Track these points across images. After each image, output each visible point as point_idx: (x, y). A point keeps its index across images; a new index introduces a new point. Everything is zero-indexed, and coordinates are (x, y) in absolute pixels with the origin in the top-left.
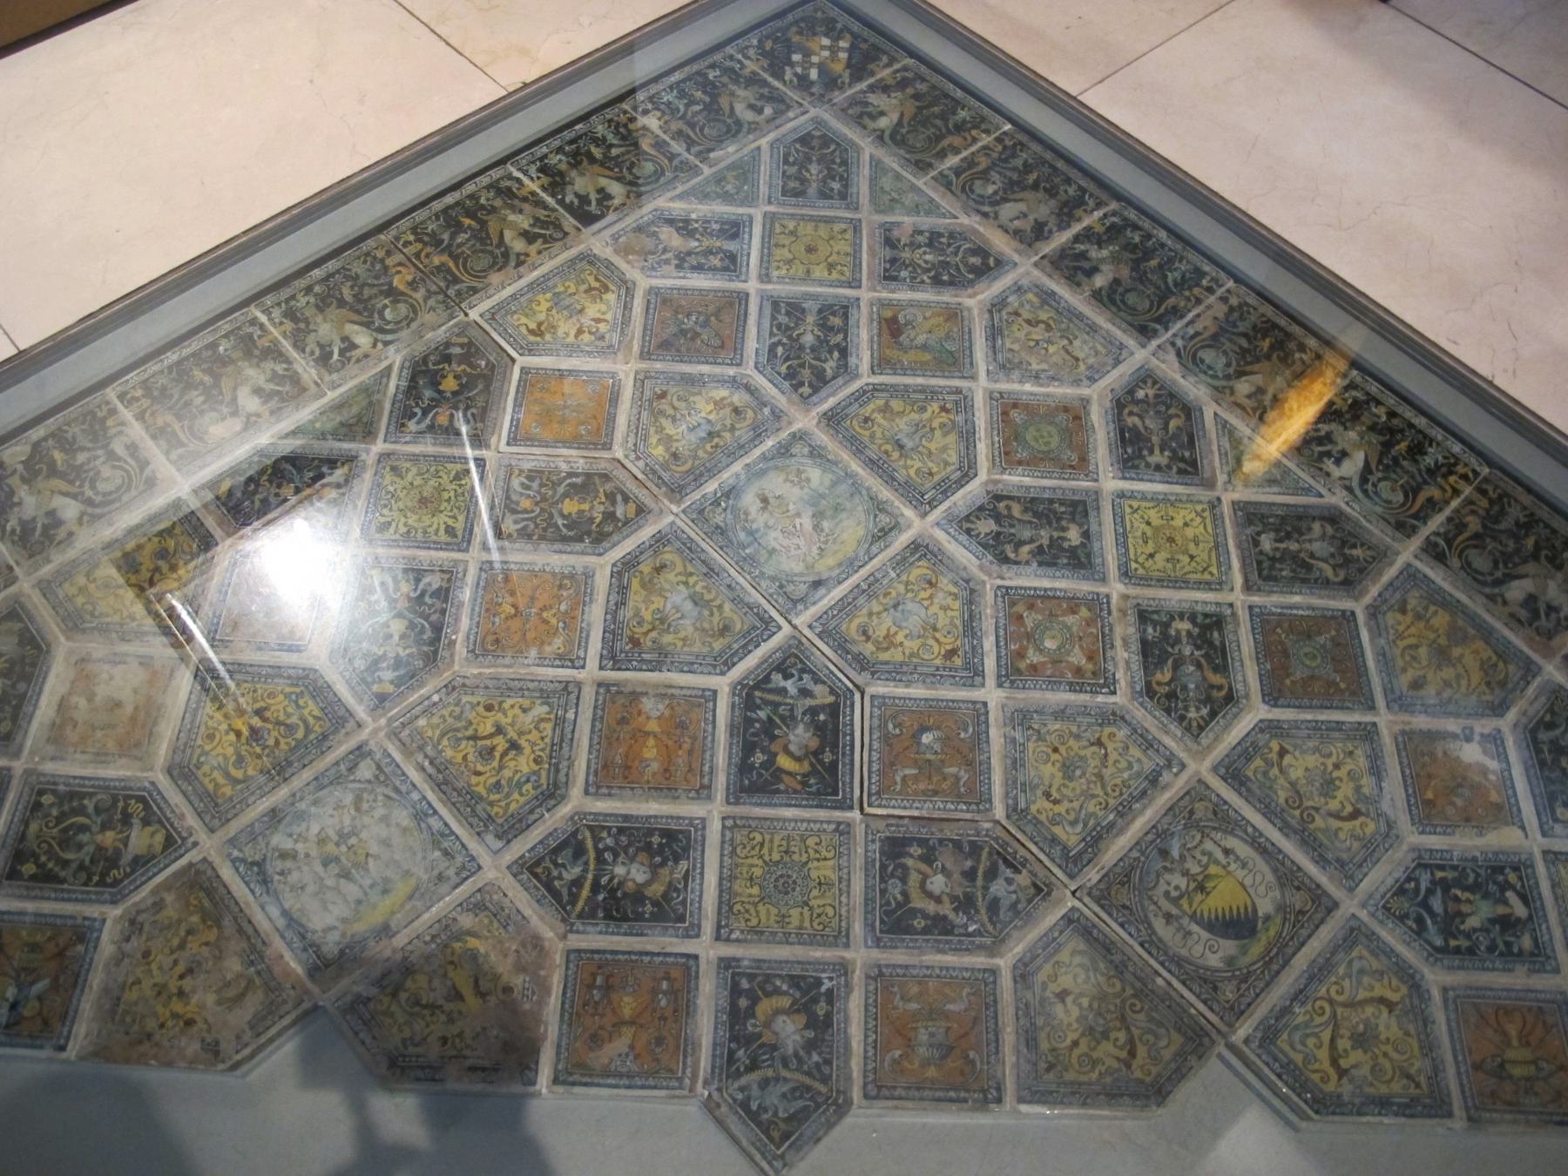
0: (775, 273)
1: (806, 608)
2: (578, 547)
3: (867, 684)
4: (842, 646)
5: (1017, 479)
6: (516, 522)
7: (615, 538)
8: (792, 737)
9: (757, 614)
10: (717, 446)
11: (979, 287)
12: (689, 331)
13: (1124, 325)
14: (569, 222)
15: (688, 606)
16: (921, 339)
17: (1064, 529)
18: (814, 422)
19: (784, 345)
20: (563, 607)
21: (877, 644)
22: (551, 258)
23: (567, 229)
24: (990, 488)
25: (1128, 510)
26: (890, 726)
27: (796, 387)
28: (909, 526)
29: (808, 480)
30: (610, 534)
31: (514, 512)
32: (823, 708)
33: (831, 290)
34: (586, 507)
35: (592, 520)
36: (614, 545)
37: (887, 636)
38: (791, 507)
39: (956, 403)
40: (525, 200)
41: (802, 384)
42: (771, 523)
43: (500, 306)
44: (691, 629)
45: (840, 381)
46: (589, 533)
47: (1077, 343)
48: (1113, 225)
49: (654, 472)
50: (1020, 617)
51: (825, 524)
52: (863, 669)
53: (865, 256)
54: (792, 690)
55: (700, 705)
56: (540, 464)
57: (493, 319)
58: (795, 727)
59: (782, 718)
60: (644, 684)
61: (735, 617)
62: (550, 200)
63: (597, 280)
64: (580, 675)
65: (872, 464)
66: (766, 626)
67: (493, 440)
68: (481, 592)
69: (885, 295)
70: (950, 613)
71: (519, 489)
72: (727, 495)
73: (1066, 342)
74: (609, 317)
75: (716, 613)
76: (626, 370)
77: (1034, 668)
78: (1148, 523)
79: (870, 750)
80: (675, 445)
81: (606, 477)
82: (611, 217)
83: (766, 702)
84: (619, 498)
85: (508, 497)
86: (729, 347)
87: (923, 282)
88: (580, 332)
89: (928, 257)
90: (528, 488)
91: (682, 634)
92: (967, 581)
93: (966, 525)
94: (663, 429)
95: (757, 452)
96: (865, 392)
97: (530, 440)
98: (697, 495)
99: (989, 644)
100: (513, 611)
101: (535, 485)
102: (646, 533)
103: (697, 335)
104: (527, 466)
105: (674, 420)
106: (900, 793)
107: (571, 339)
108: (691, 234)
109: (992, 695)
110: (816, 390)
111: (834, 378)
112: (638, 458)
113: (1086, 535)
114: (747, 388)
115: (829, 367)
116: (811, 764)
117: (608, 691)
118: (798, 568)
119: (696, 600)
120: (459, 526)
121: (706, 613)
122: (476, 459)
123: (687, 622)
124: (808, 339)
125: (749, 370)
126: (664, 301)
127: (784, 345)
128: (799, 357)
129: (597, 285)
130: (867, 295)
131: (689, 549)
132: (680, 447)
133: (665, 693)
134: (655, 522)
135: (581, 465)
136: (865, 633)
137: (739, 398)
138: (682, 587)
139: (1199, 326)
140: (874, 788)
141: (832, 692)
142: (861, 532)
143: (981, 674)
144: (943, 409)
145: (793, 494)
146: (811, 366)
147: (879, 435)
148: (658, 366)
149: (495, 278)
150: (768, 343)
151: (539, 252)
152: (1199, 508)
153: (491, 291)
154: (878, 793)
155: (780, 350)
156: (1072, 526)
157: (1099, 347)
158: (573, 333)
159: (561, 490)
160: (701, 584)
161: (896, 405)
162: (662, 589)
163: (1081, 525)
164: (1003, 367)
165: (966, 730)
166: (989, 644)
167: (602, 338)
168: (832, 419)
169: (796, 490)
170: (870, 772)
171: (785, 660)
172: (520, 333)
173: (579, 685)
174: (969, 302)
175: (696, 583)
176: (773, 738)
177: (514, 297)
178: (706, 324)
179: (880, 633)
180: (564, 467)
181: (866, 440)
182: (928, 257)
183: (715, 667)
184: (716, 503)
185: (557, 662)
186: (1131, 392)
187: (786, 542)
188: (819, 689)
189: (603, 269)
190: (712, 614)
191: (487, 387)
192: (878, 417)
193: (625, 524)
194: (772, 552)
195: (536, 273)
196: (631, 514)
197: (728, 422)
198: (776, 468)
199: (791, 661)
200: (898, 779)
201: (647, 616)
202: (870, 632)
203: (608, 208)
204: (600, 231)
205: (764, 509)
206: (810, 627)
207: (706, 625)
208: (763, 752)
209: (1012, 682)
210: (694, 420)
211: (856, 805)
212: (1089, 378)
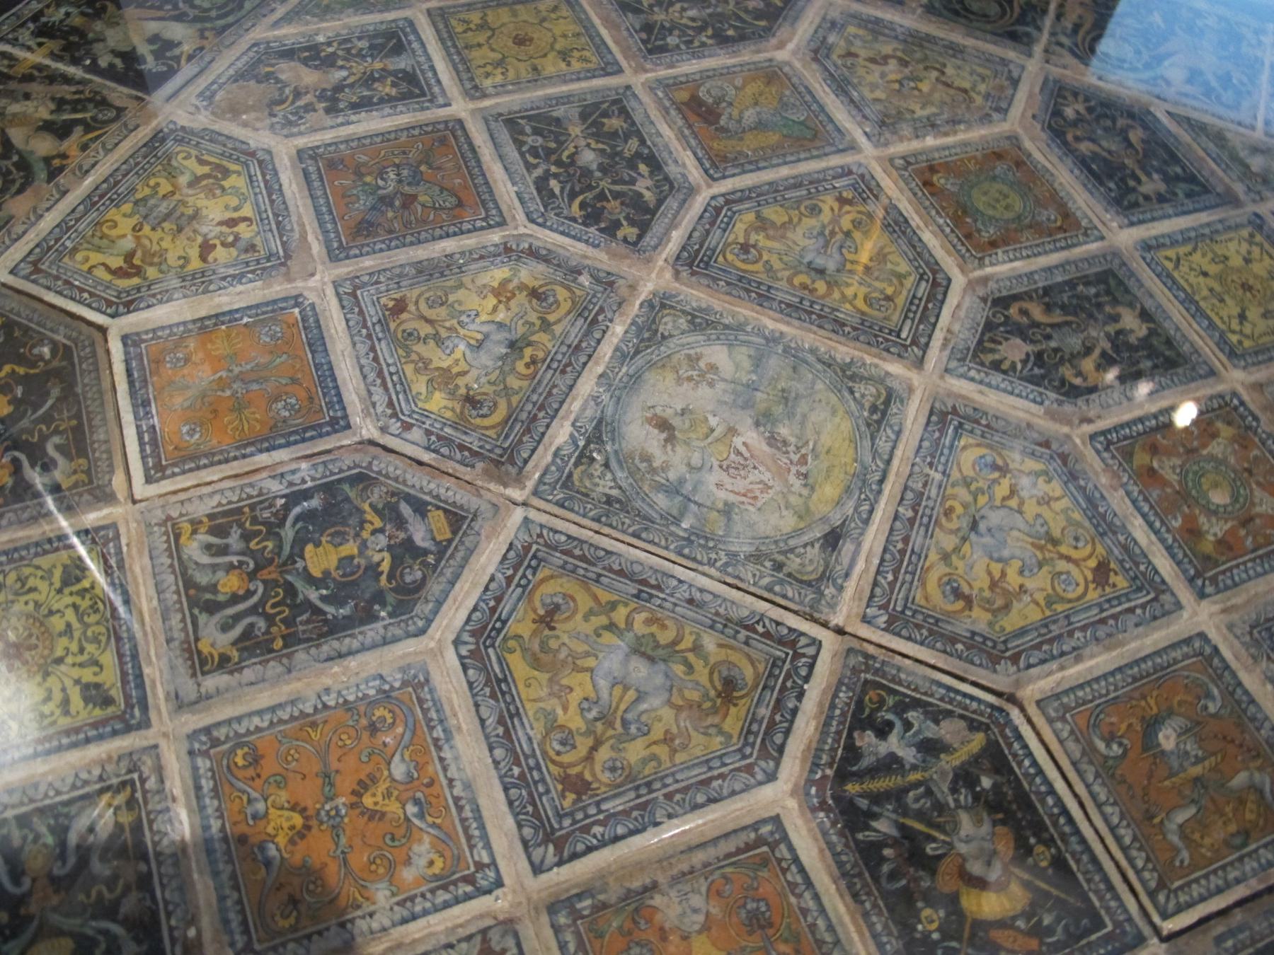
0: (488, 83)
1: (841, 589)
2: (372, 632)
3: (1018, 684)
4: (934, 631)
5: (1003, 269)
6: (225, 628)
7: (435, 588)
8: (962, 848)
9: (767, 635)
10: (534, 361)
11: (783, 32)
12: (398, 196)
13: (989, 37)
14: (119, 93)
15: (640, 670)
16: (750, 116)
17: (1116, 318)
18: (668, 275)
19: (556, 176)
20: (399, 769)
21: (987, 605)
22: (108, 151)
23: (118, 103)
24: (981, 292)
25: (1169, 265)
26: (1101, 746)
27: (611, 230)
28: (911, 390)
29: (713, 368)
30: (420, 586)
31: (212, 608)
32: (976, 760)
33: (584, 84)
34: (351, 548)
35: (373, 570)
36: (439, 604)
37: (993, 585)
38: (713, 421)
39: (854, 187)
40: (28, 78)
41: (617, 225)
42: (696, 459)
43: (44, 247)
44: (667, 714)
45: (672, 203)
46: (379, 597)
47: (949, 71)
49: (447, 441)
50: (1152, 472)
51: (784, 431)
52: (994, 660)
53: (604, 32)
54: (909, 755)
55: (764, 862)
56: (229, 496)
57: (37, 270)
58: (956, 825)
59: (920, 815)
60: (640, 866)
61: (735, 657)
62: (72, 70)
63: (202, 162)
64: (498, 903)
65: (792, 310)
66: (792, 657)
67: (118, 481)
68: (211, 804)
69: (663, 73)
70: (1058, 506)
71: (205, 559)
72: (596, 438)
73: (935, 74)
74: (247, 211)
75: (698, 664)
76: (319, 284)
77: (1224, 544)
78: (1205, 274)
79: (1099, 806)
80: (461, 382)
81: (362, 480)
82: (187, 70)
83: (877, 798)
84: (405, 509)
85: (189, 583)
86: (468, 202)
87: (703, 45)
88: (206, 249)
89: (691, 13)
90: (224, 551)
91: (657, 733)
92: (1046, 444)
93: (989, 358)
94: (426, 363)
95: (606, 350)
96: (718, 210)
97: (191, 459)
98: (544, 457)
99: (1139, 531)
100: (298, 820)
101: (234, 540)
102: (487, 560)
103: (409, 200)
104: (201, 509)
105: (439, 341)
106: (1194, 867)
107: (196, 264)
108: (329, 62)
109: (1200, 616)
110: (644, 228)
111: (660, 202)
112: (407, 427)
113: (1145, 315)
114: (533, 253)
115: (645, 187)
116: (1027, 885)
117: (576, 915)
118: (788, 522)
119: (645, 650)
120: (110, 677)
121: (679, 669)
122: (83, 533)
123: (655, 701)
125: (521, 227)
126: (331, 165)
127: (556, 176)
128: (590, 188)
129: (206, 169)
130: (639, 80)
131: (583, 562)
132: (474, 382)
133: (681, 867)
134: (494, 533)
135: (306, 473)
136: (957, 594)
137: (529, 273)
138: (608, 638)
140: (1151, 878)
141: (974, 726)
142: (847, 426)
143: (1161, 587)
145: (703, 397)
146: (617, 195)
147: (777, 265)
148: (368, 263)
150: (530, 180)
151: (84, 147)
152: (1245, 233)
153: (19, 229)
154: (1162, 885)
155: (554, 184)
156: (1121, 310)
157: (980, 70)
158: (194, 253)
159: (288, 533)
160: (640, 618)
161: (773, 213)
162: (573, 655)
163: (1131, 305)
164: (882, 124)
165: (1209, 695)
166: (1139, 531)
167: (252, 248)
168: (694, 260)
169: (704, 391)
170: (1124, 849)
171: (860, 704)
172: (98, 282)
173: (509, 925)
174: (782, 55)
175: (629, 622)
176: (932, 865)
177: (63, 227)
178: (417, 178)
179: (980, 582)
180: (275, 487)
181: (763, 277)
182: (691, 13)
183: (749, 769)
184: (584, 458)
185: (442, 896)
187: (741, 485)
188: (948, 730)
189: (206, 144)
190: (690, 668)
191: (69, 394)
192: (758, 238)
193: (440, 554)
194: (727, 511)
195: (89, 182)
196: (444, 533)
197: (533, 317)
198: (651, 365)
199: (871, 702)
200: (1175, 839)
201: (575, 722)
202: (966, 590)
203: (177, 59)
204: (175, 94)
205: (671, 439)
206: (866, 620)
207: (695, 696)
208: (929, 903)
209: (1214, 580)
210: (474, 330)
211: (1147, 930)
212: (998, 110)
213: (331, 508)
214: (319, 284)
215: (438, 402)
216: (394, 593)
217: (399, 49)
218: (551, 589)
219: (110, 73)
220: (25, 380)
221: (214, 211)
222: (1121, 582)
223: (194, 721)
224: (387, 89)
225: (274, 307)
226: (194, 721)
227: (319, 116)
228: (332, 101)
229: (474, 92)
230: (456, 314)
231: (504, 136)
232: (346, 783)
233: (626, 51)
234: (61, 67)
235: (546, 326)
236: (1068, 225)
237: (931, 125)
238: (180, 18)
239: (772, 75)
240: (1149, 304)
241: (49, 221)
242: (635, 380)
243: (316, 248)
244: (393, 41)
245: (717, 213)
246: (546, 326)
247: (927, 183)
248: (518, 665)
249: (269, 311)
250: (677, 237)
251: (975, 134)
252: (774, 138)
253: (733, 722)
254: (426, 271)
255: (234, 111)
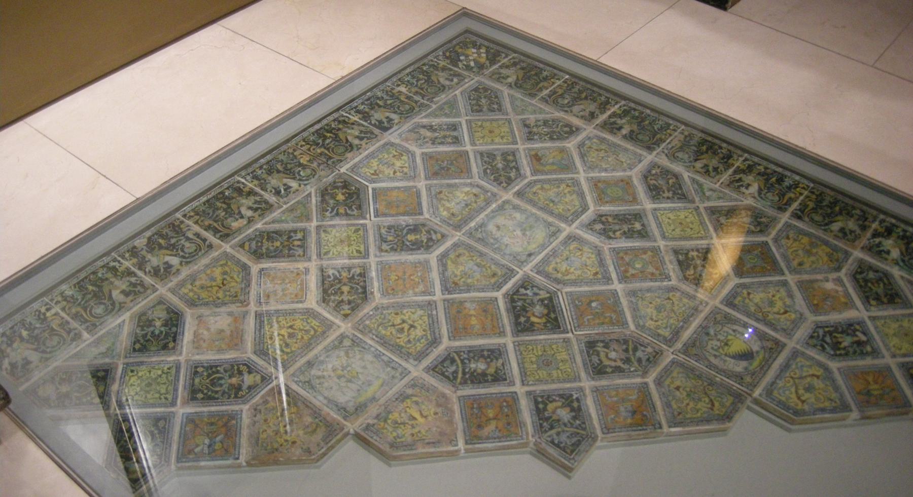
2: (419, 252)
4: (547, 276)
7: (435, 247)
11: (572, 138)
14: (377, 131)
15: (476, 268)
16: (551, 161)
34: (418, 237)
35: (422, 241)
40: (353, 124)
43: (355, 166)
46: (422, 246)
48: (625, 110)
62: (364, 123)
65: (541, 209)
66: (511, 273)
67: (368, 216)
72: (481, 226)
74: (407, 165)
81: (424, 225)
86: (465, 171)
88: (395, 172)
95: (489, 210)
97: (385, 215)
98: (467, 228)
99: (611, 269)
102: (448, 244)
103: (448, 169)
105: (448, 201)
108: (435, 130)
109: (618, 286)
110: (509, 184)
114: (478, 186)
115: (513, 175)
118: (520, 250)
119: (478, 265)
120: (362, 249)
124: (500, 166)
125: (477, 180)
126: (430, 158)
130: (522, 147)
133: (473, 301)
137: (475, 190)
139: (673, 144)
144: (567, 186)
145: (509, 223)
148: (435, 182)
149: (349, 155)
155: (488, 171)
159: (405, 231)
167: (406, 174)
177: (360, 162)
178: (452, 164)
180: (403, 223)
184: (476, 230)
186: (649, 171)
192: (540, 192)
194: (507, 245)
201: (458, 273)
213: (415, 229)
214: (422, 185)
215: (445, 213)
216: (428, 246)
217: (455, 129)
218: (461, 250)
219: (375, 125)
220: (349, 194)
221: (398, 164)
222: (600, 276)
223: (377, 259)
224: (449, 140)
225: (410, 188)
226: (377, 259)
227: (429, 144)
228: (434, 141)
229: (473, 144)
230: (454, 196)
231: (479, 157)
232: (408, 274)
233: (521, 138)
234: (362, 122)
235: (476, 202)
236: (635, 200)
237: (606, 170)
238: (395, 113)
239: (562, 150)
240: (646, 223)
241: (357, 160)
242: (493, 217)
243: (423, 176)
244: (454, 127)
245: (530, 184)
246: (476, 202)
247: (596, 185)
248: (449, 262)
249: (407, 189)
250: (517, 188)
251: (619, 174)
252: (555, 167)
253: (493, 280)
254: (449, 186)
255: (407, 140)
